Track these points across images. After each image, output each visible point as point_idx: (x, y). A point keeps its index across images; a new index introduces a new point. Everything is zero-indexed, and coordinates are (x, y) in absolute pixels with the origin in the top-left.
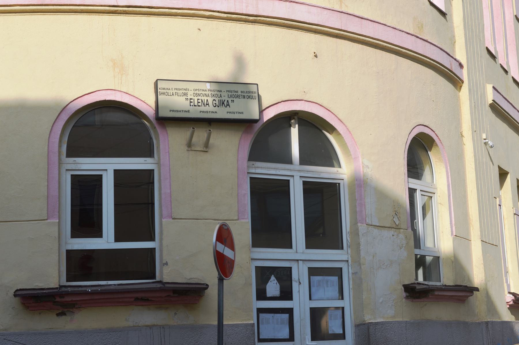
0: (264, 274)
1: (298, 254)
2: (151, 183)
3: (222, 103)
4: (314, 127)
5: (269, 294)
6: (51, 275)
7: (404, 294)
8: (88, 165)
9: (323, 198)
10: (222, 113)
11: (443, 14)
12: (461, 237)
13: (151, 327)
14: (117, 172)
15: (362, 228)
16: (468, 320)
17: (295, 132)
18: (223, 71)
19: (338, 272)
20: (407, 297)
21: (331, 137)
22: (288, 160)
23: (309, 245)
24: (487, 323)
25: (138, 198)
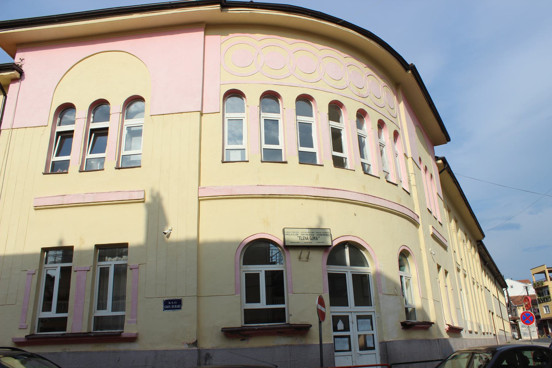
0: (335, 319)
1: (351, 309)
2: (525, 320)
3: (314, 238)
4: (356, 248)
5: (339, 329)
6: (238, 321)
7: (401, 327)
8: (253, 269)
9: (362, 281)
10: (314, 243)
11: (441, 224)
12: (424, 299)
13: (285, 345)
14: (266, 272)
15: (380, 295)
16: (430, 338)
17: (347, 251)
18: (313, 224)
19: (370, 317)
20: (403, 328)
21: (363, 253)
22: (345, 264)
23: (357, 304)
24: (438, 339)
25: (276, 281)
